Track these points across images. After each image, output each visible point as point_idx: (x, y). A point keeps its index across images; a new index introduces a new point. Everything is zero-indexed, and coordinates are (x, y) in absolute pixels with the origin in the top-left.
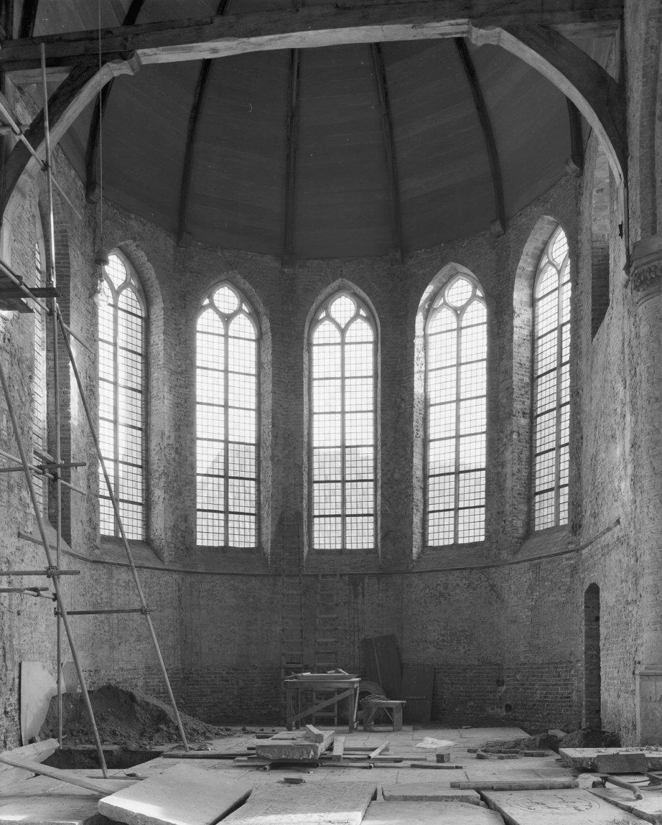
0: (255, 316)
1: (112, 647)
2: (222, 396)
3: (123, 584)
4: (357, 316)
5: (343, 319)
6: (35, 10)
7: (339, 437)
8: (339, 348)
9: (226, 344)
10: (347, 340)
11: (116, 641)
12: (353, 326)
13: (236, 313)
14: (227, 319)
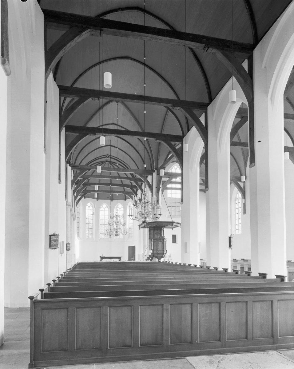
4: (106, 207)
14: (89, 207)
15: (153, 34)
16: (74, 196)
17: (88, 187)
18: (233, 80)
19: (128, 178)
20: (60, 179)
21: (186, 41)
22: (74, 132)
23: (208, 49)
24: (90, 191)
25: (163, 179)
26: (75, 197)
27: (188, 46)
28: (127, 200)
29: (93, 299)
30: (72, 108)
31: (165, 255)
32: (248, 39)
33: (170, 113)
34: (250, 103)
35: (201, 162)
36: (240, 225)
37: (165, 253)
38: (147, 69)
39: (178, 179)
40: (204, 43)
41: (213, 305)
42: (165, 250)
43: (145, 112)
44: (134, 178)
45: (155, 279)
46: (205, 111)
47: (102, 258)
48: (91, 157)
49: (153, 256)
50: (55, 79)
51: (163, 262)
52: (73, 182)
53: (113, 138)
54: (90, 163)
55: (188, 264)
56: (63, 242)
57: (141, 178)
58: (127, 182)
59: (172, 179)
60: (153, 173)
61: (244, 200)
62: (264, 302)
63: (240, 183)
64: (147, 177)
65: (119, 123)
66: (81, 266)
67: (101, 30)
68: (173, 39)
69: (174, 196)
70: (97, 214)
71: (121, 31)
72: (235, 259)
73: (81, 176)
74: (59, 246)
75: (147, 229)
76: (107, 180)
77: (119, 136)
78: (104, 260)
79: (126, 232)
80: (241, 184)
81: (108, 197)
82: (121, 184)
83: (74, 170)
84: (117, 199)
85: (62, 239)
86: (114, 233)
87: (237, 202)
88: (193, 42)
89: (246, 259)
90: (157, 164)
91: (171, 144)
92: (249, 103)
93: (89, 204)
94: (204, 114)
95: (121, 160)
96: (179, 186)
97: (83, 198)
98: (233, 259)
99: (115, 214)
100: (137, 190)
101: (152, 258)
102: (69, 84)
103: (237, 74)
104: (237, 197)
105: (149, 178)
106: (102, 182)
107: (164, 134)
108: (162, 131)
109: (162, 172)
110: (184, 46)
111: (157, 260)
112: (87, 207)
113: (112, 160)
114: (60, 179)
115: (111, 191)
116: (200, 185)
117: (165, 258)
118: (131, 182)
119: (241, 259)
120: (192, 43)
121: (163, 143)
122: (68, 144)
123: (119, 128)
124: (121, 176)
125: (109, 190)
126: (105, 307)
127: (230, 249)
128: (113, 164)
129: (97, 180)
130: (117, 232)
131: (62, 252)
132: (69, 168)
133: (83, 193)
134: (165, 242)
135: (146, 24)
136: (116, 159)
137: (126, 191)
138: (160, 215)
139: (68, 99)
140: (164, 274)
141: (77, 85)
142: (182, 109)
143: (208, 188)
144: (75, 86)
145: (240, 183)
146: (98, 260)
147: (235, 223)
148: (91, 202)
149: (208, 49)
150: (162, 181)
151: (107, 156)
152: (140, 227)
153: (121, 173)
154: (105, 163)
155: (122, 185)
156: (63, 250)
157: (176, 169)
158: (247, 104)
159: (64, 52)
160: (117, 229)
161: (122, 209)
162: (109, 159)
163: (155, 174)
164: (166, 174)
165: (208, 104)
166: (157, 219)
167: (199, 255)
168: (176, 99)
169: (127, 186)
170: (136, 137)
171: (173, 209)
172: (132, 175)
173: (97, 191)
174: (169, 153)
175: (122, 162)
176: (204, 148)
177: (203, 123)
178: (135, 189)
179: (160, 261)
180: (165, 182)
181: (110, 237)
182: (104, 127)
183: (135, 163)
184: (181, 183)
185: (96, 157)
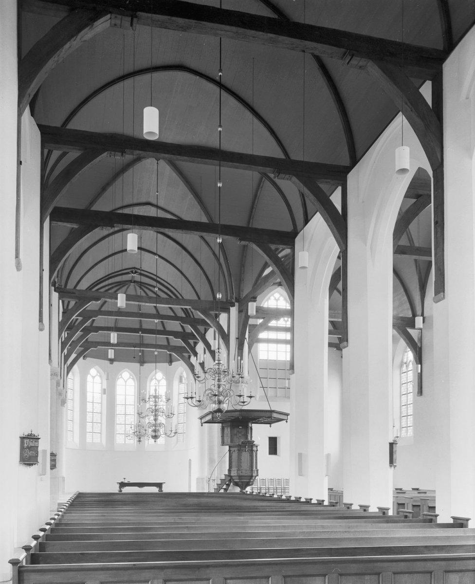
2: (92, 399)
4: (130, 378)
6: (80, 131)
7: (124, 412)
8: (127, 404)
9: (93, 405)
14: (94, 377)
15: (239, 26)
16: (63, 354)
17: (92, 336)
18: (400, 124)
19: (176, 318)
20: (41, 320)
21: (306, 42)
22: (68, 222)
23: (350, 60)
24: (96, 344)
25: (251, 321)
26: (65, 356)
27: (311, 52)
28: (173, 363)
29: (134, 565)
30: (69, 173)
31: (254, 480)
32: (434, 40)
33: (267, 184)
34: (436, 170)
35: (333, 287)
36: (410, 419)
37: (254, 475)
38: (224, 93)
39: (285, 322)
40: (343, 47)
41: (367, 577)
42: (254, 469)
43: (219, 185)
44: (187, 318)
45: (244, 528)
46: (341, 182)
47: (122, 485)
48: (99, 272)
49: (229, 480)
50: (32, 114)
51: (251, 494)
52: (61, 325)
53: (150, 233)
54: (96, 285)
55: (318, 500)
56: (45, 451)
57: (206, 319)
58: (174, 326)
59: (269, 320)
60: (231, 308)
61: (420, 366)
62: (467, 573)
63: (410, 331)
64: (217, 316)
65: (161, 204)
66: (80, 501)
67: (133, 17)
68: (281, 38)
69: (272, 357)
70: (109, 392)
71: (174, 18)
72: (401, 489)
73: (79, 314)
74: (40, 459)
75: (216, 424)
76: (132, 322)
77: (162, 230)
78: (126, 490)
79: (174, 431)
80: (413, 332)
81: (134, 358)
82: (162, 329)
83: (63, 299)
84: (156, 360)
85: (44, 446)
86: (150, 431)
87: (404, 369)
88: (321, 43)
89: (422, 488)
90: (239, 290)
91: (270, 249)
92: (433, 171)
93: (93, 371)
94: (340, 189)
95: (164, 280)
96: (287, 336)
97: (82, 357)
98: (396, 489)
99: (152, 393)
100: (196, 344)
101: (228, 485)
102: (57, 123)
103: (410, 110)
104: (405, 360)
105: (223, 318)
106: (120, 325)
107: (256, 229)
108: (249, 222)
109: (252, 308)
110: (304, 51)
111: (238, 490)
112: (89, 378)
113: (145, 280)
114: (41, 320)
115: (142, 345)
116: (329, 334)
117: (253, 486)
118: (182, 327)
119: (413, 489)
120: (319, 46)
121: (255, 247)
122: (55, 248)
123: (161, 214)
124: (161, 313)
125: (138, 341)
126: (156, 580)
127: (393, 468)
128: (147, 288)
129: (110, 320)
130: (155, 431)
131: (44, 473)
132: (55, 295)
133: (82, 348)
134: (254, 453)
135: (222, 6)
136: (155, 277)
137: (172, 344)
138: (251, 397)
139: (56, 154)
140: (261, 519)
141: (76, 124)
142: (294, 179)
143: (347, 341)
144: (71, 126)
145: (410, 331)
146: (115, 489)
147: (401, 413)
148: (97, 367)
149: (350, 60)
150: (250, 325)
151: (134, 270)
152: (203, 420)
153: (163, 307)
154: (127, 286)
155: (164, 332)
156: (44, 469)
157: (277, 300)
158: (430, 172)
159: (58, 61)
160: (155, 425)
161: (164, 382)
162: (137, 277)
163: (234, 311)
164: (259, 310)
165: (349, 169)
166: (243, 406)
167: (326, 479)
168: (282, 156)
169: (176, 334)
170: (198, 233)
171: (271, 383)
172: (185, 311)
173: (113, 345)
174: (266, 266)
175: (166, 284)
176: (339, 257)
177: (339, 207)
178: (191, 342)
179: (244, 491)
180: (254, 326)
181: (140, 441)
182: (127, 211)
183: (193, 287)
184: (291, 330)
185: (107, 274)
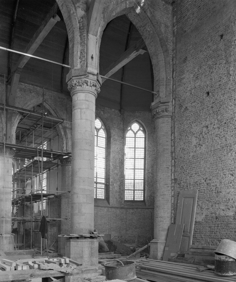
0: (144, 131)
1: (127, 230)
3: (131, 213)
5: (135, 130)
10: (136, 136)
11: (128, 229)
12: (138, 132)
13: (100, 129)
